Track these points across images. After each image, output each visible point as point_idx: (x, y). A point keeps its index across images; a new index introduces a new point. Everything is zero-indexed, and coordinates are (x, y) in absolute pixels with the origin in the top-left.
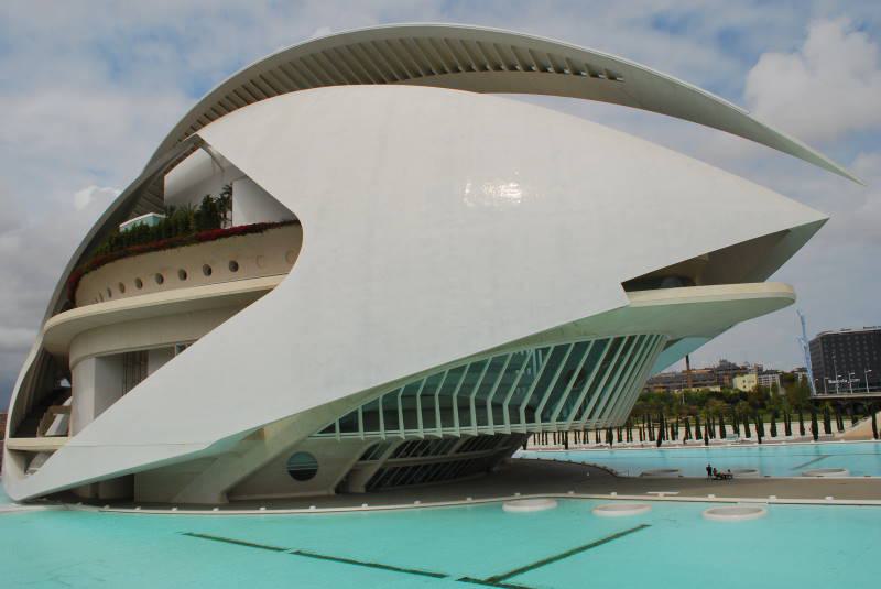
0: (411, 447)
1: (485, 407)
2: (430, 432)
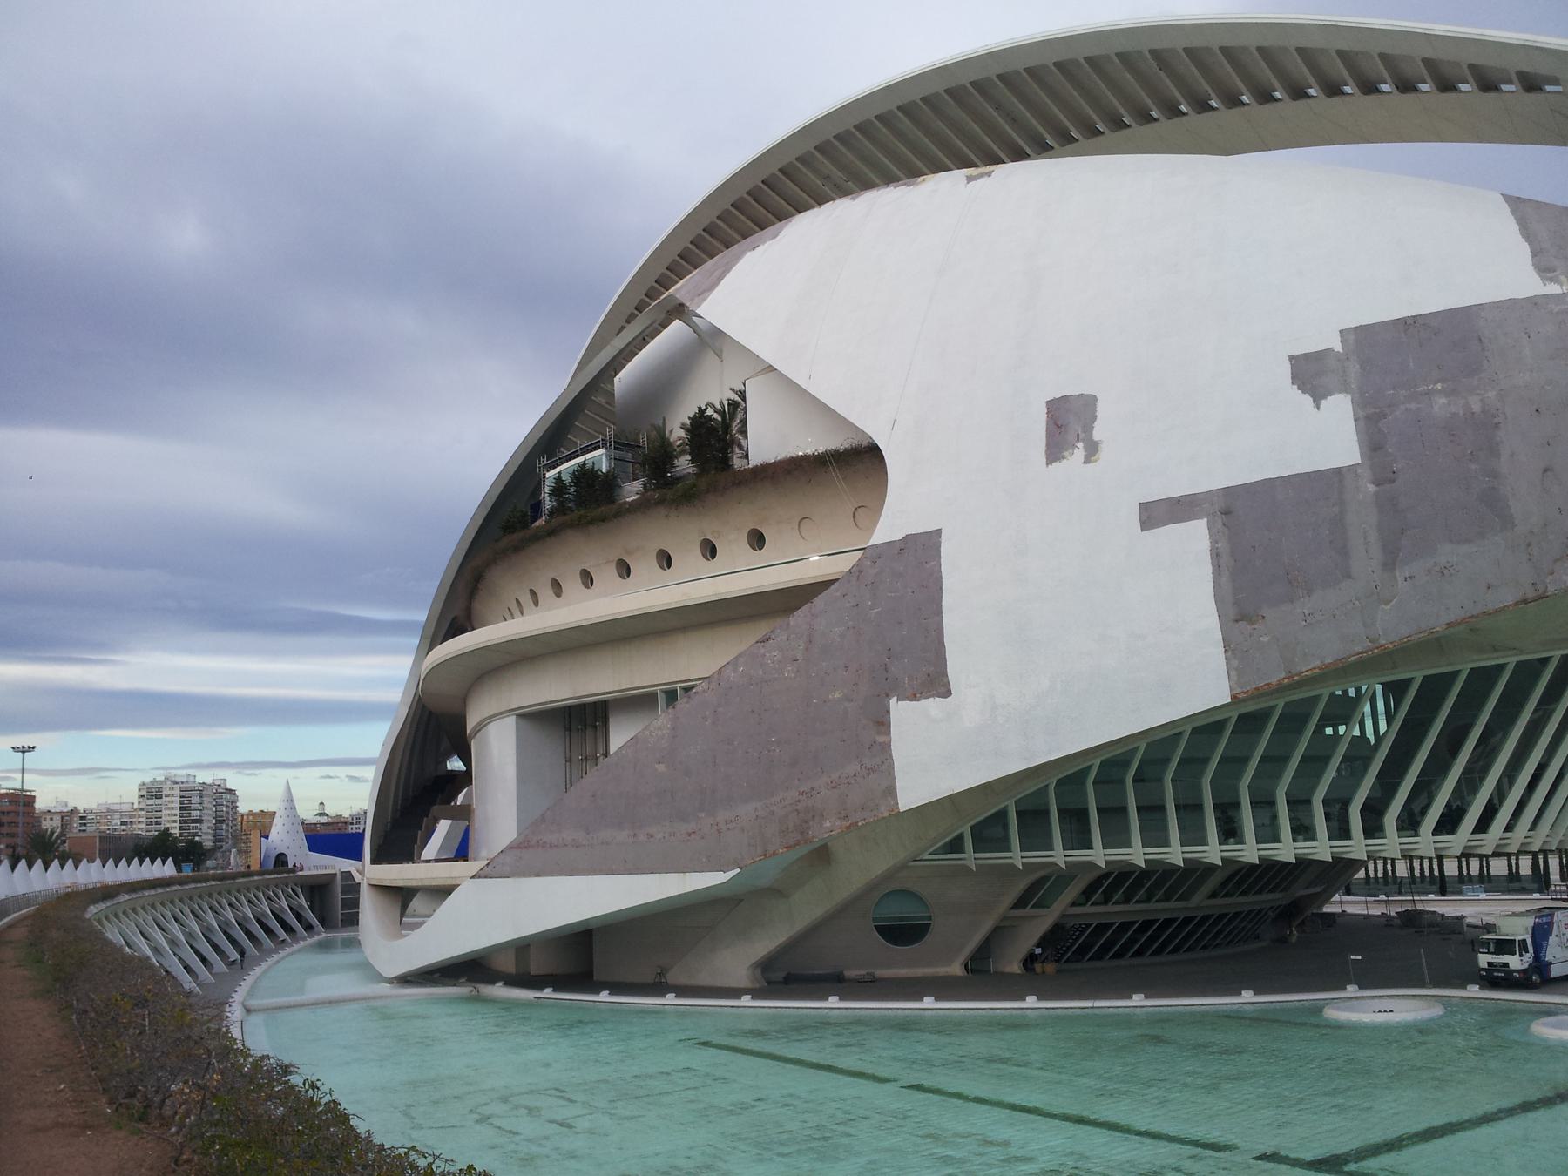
0: (1119, 881)
1: (1272, 803)
2: (1156, 853)
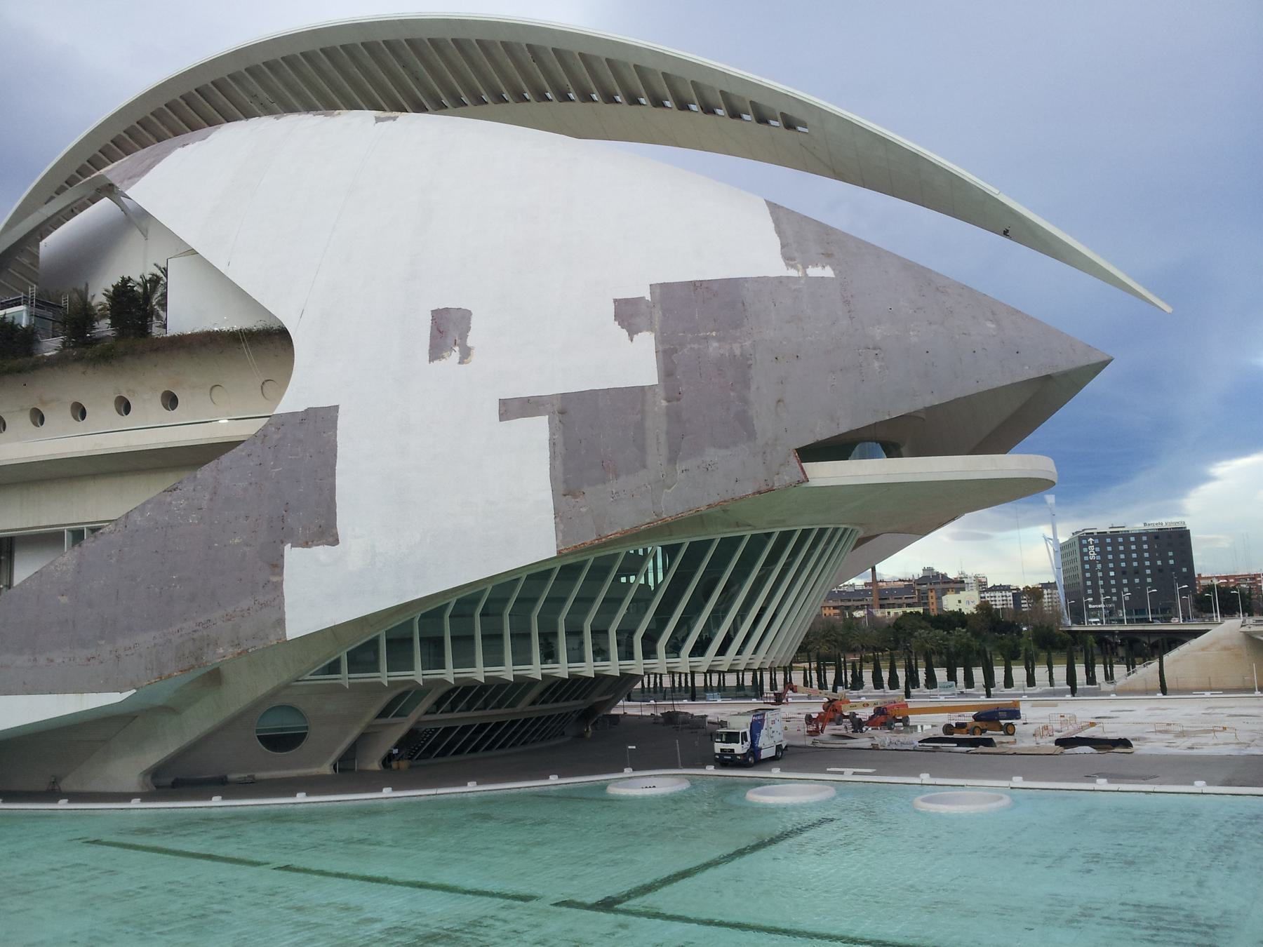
0: (465, 693)
2: (465, 673)
